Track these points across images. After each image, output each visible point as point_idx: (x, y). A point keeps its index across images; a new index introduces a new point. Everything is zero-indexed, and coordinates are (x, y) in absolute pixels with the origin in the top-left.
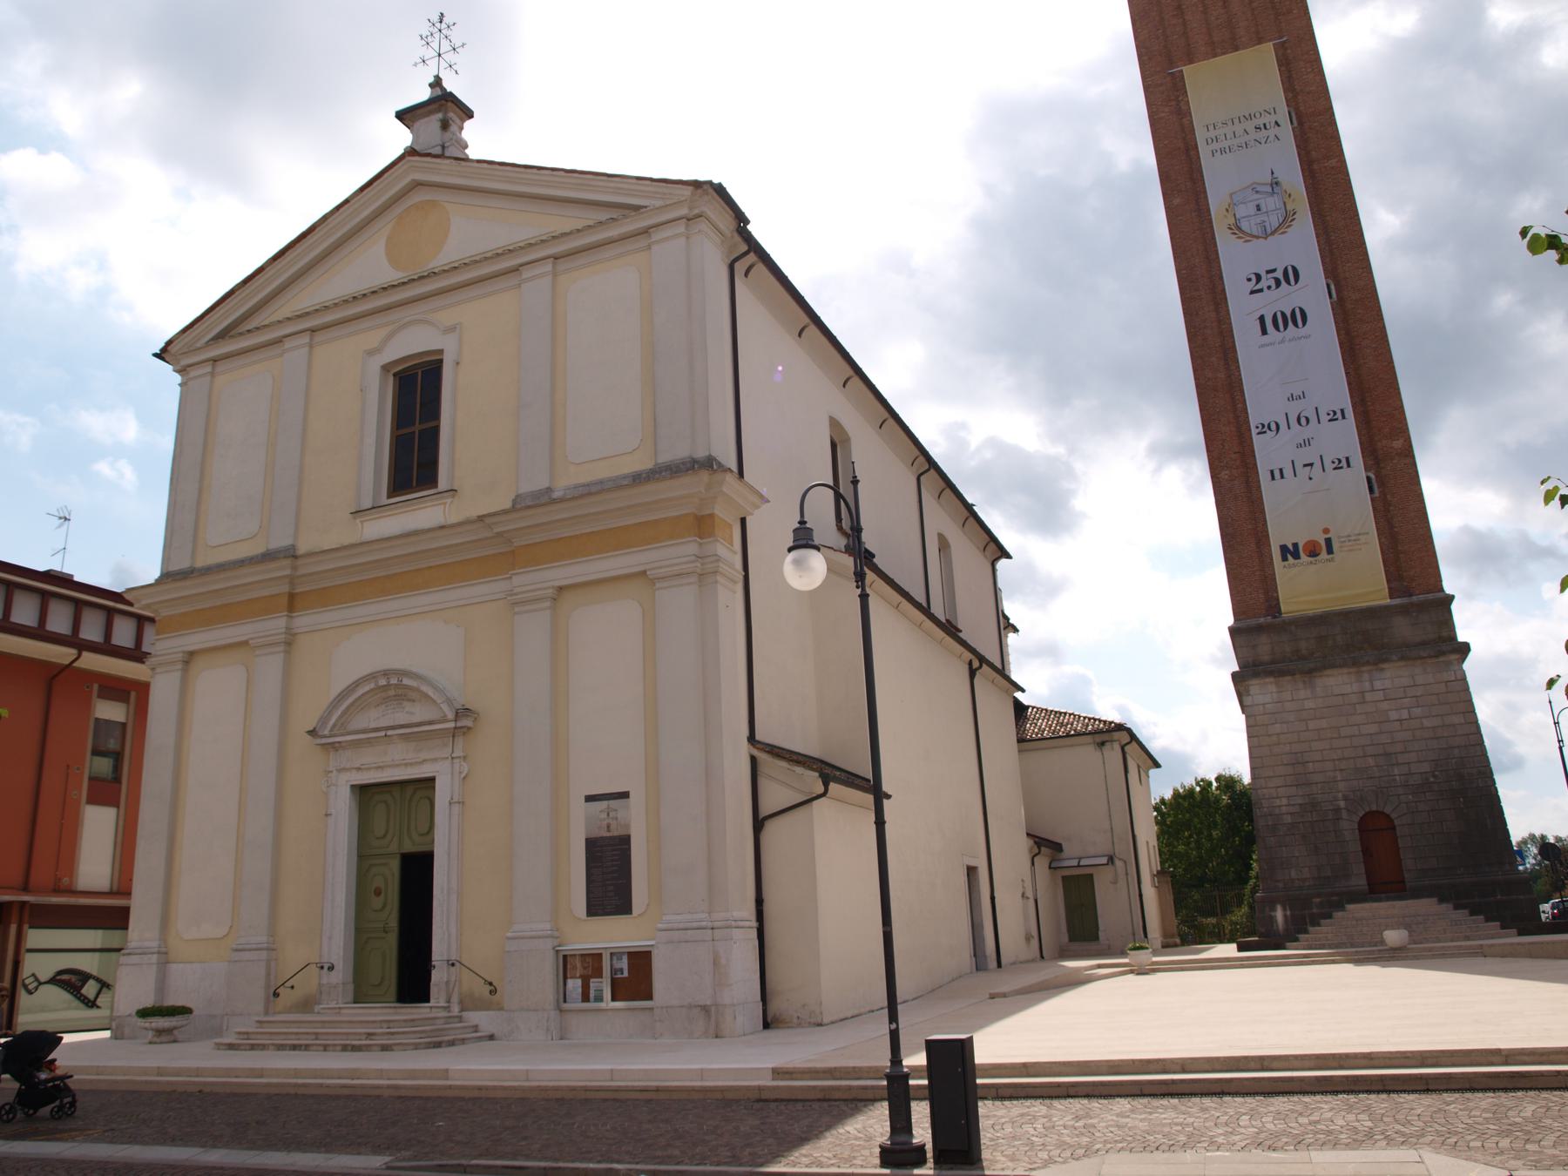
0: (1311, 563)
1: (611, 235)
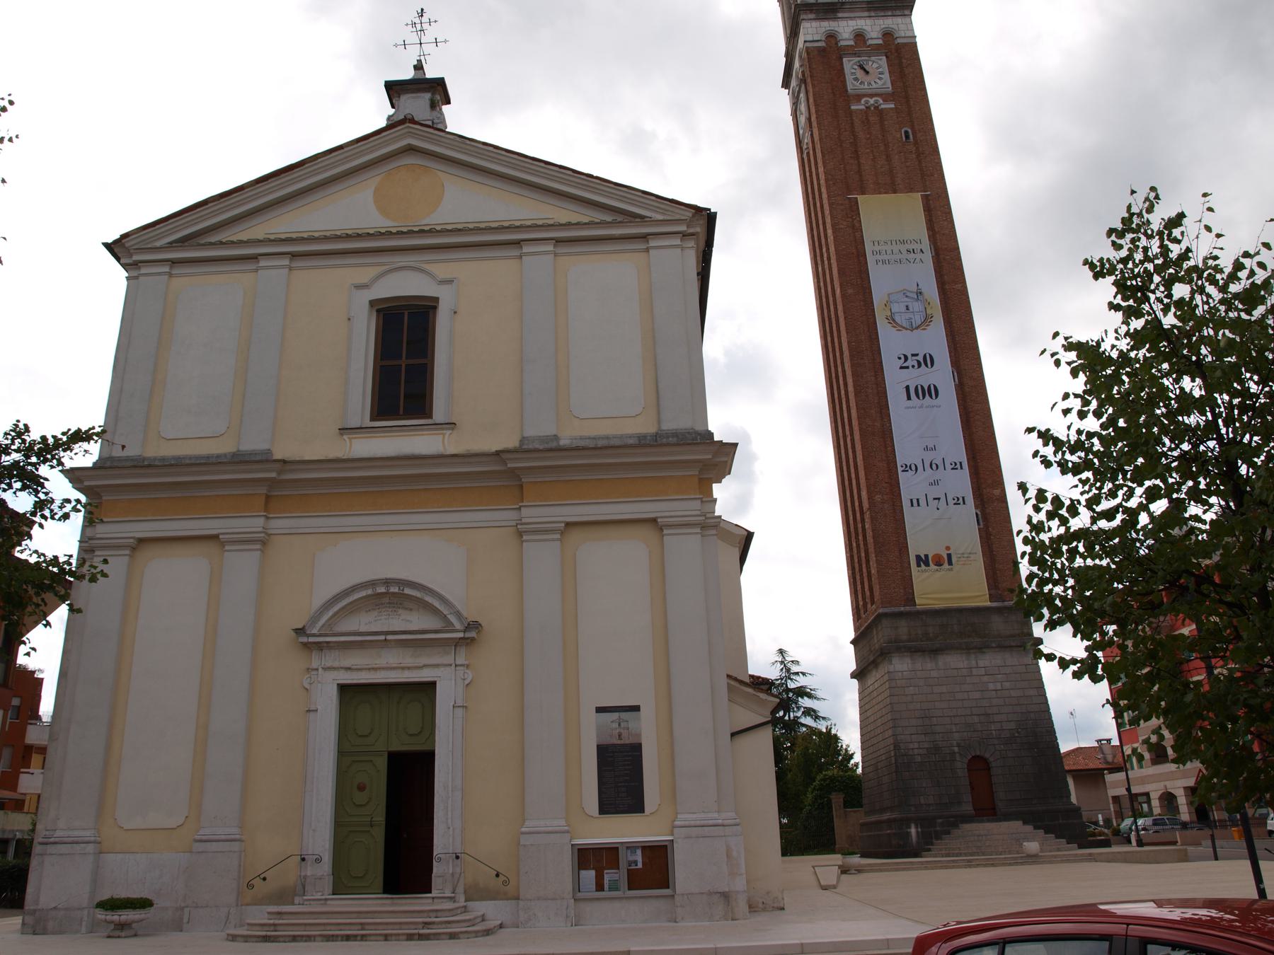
1: (614, 233)
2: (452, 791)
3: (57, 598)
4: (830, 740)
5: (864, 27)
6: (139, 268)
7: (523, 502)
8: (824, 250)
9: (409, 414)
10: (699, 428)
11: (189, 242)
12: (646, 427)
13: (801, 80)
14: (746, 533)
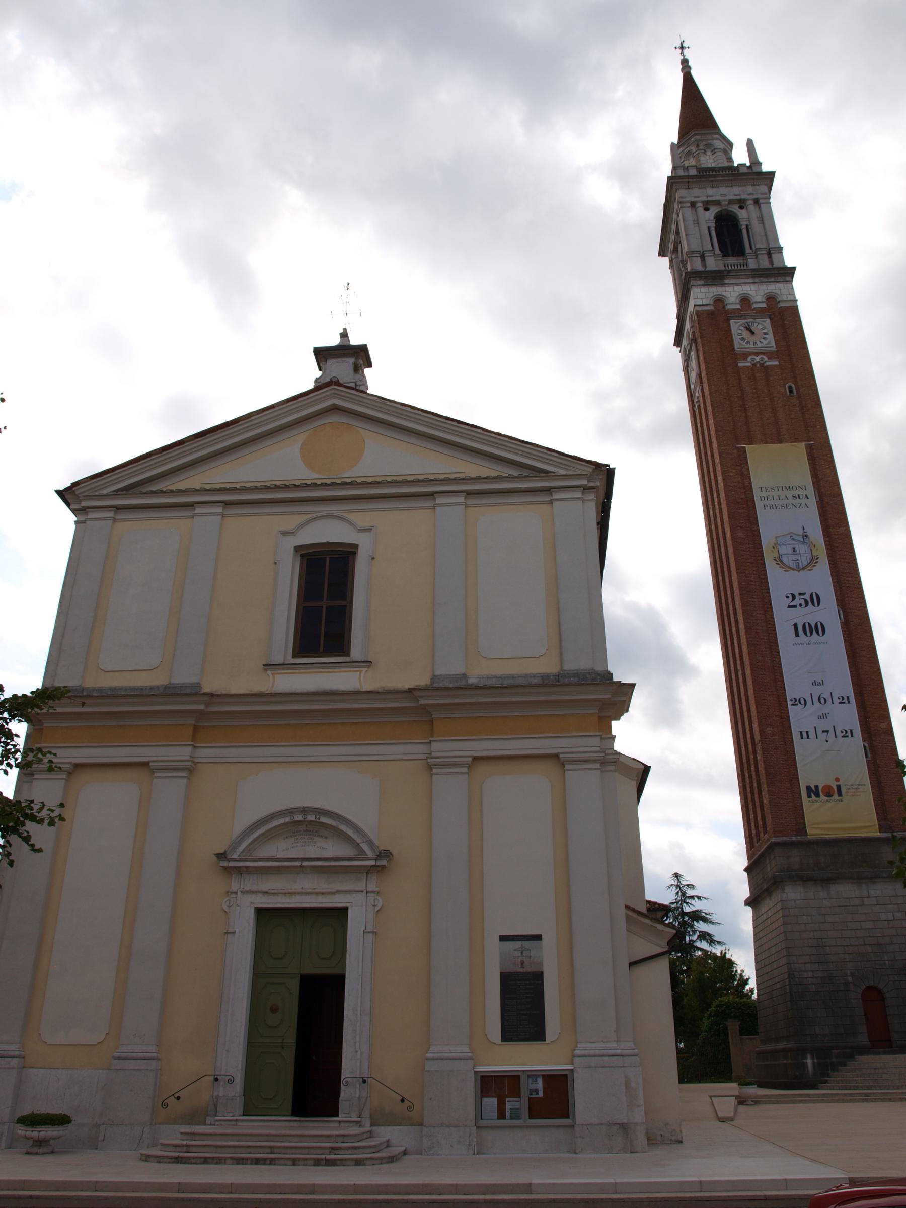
0: (827, 801)
2: (361, 1015)
3: (20, 839)
4: (726, 964)
5: (750, 292)
6: (87, 514)
7: (433, 737)
8: (715, 495)
9: (328, 652)
10: (599, 668)
11: (132, 490)
12: (549, 666)
13: (692, 339)
14: (643, 767)
